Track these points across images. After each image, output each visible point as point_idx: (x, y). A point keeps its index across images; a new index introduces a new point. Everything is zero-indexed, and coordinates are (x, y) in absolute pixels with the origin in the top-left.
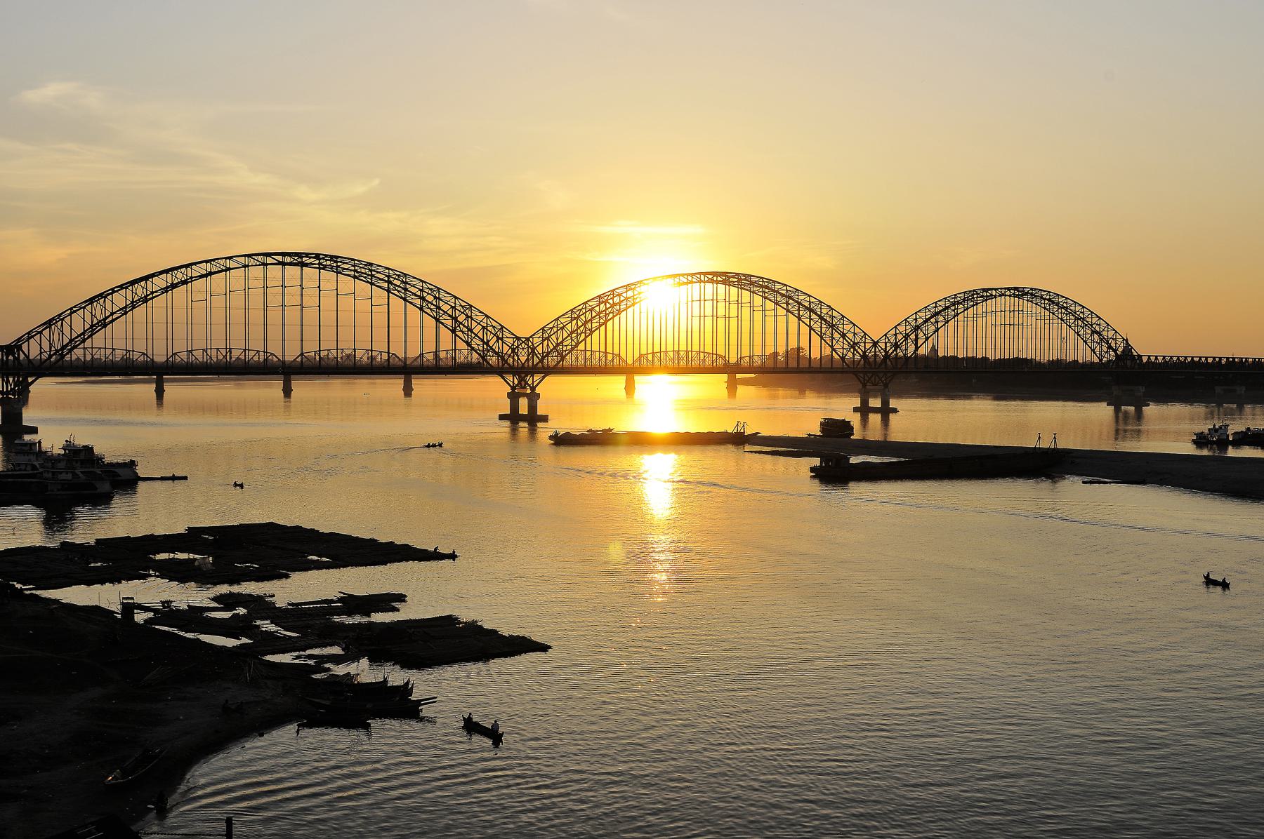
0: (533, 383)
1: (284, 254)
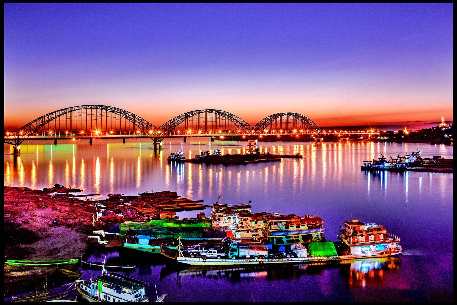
0: (160, 140)
1: (92, 106)
